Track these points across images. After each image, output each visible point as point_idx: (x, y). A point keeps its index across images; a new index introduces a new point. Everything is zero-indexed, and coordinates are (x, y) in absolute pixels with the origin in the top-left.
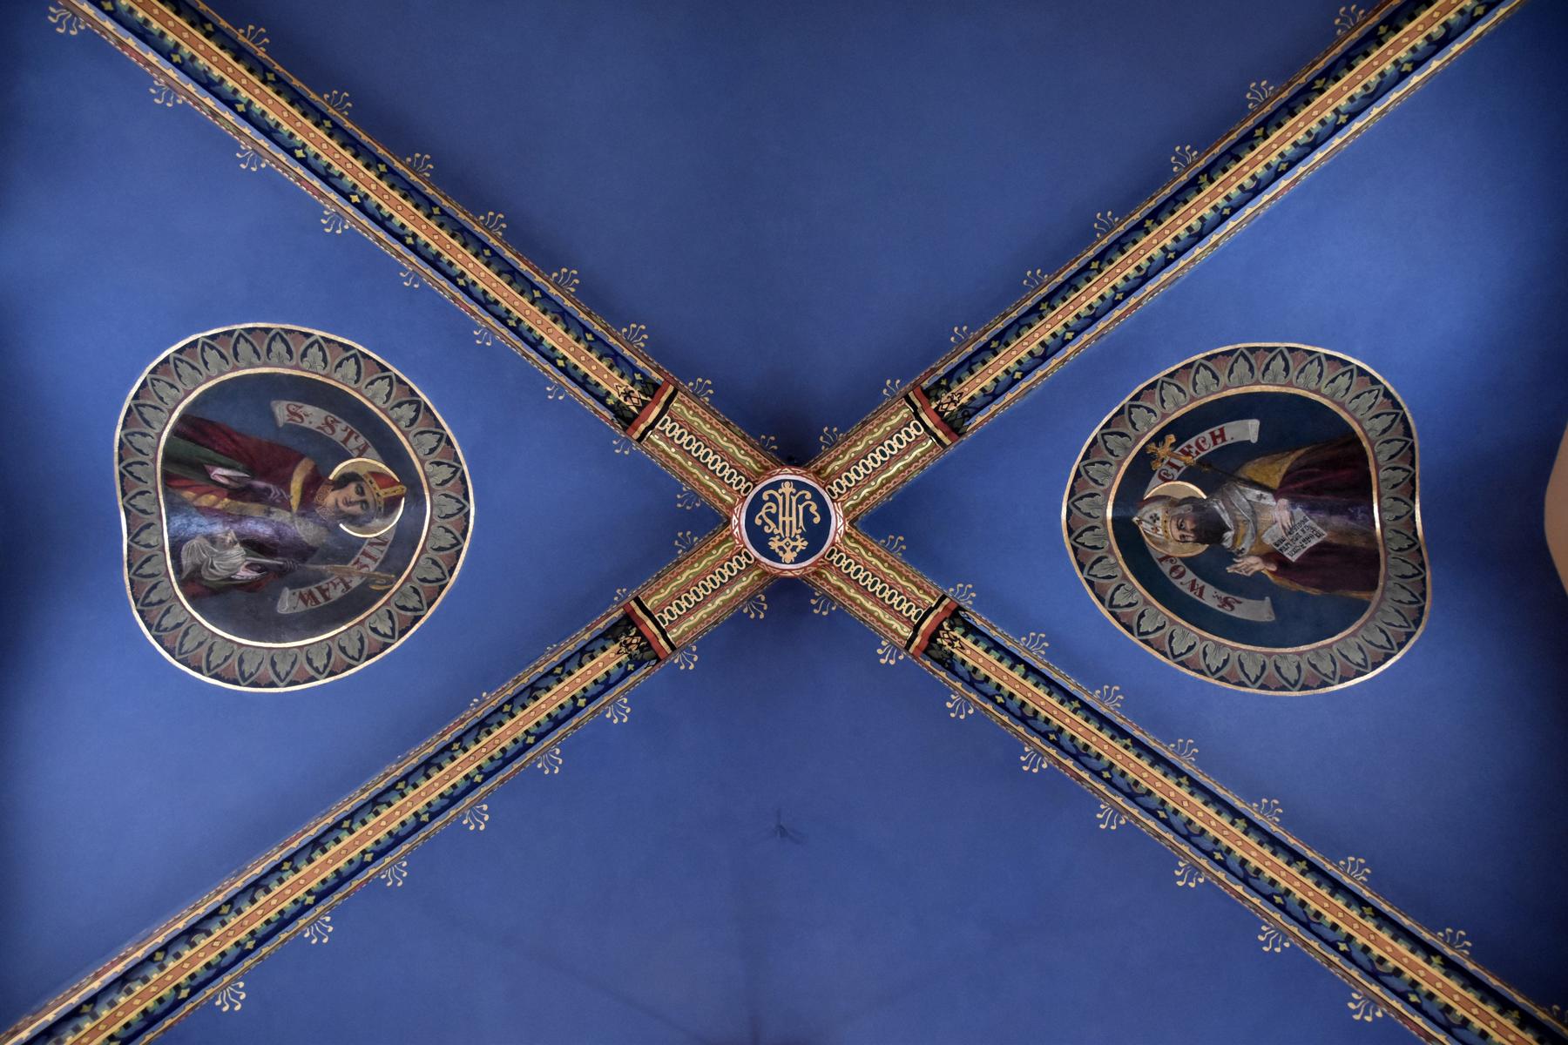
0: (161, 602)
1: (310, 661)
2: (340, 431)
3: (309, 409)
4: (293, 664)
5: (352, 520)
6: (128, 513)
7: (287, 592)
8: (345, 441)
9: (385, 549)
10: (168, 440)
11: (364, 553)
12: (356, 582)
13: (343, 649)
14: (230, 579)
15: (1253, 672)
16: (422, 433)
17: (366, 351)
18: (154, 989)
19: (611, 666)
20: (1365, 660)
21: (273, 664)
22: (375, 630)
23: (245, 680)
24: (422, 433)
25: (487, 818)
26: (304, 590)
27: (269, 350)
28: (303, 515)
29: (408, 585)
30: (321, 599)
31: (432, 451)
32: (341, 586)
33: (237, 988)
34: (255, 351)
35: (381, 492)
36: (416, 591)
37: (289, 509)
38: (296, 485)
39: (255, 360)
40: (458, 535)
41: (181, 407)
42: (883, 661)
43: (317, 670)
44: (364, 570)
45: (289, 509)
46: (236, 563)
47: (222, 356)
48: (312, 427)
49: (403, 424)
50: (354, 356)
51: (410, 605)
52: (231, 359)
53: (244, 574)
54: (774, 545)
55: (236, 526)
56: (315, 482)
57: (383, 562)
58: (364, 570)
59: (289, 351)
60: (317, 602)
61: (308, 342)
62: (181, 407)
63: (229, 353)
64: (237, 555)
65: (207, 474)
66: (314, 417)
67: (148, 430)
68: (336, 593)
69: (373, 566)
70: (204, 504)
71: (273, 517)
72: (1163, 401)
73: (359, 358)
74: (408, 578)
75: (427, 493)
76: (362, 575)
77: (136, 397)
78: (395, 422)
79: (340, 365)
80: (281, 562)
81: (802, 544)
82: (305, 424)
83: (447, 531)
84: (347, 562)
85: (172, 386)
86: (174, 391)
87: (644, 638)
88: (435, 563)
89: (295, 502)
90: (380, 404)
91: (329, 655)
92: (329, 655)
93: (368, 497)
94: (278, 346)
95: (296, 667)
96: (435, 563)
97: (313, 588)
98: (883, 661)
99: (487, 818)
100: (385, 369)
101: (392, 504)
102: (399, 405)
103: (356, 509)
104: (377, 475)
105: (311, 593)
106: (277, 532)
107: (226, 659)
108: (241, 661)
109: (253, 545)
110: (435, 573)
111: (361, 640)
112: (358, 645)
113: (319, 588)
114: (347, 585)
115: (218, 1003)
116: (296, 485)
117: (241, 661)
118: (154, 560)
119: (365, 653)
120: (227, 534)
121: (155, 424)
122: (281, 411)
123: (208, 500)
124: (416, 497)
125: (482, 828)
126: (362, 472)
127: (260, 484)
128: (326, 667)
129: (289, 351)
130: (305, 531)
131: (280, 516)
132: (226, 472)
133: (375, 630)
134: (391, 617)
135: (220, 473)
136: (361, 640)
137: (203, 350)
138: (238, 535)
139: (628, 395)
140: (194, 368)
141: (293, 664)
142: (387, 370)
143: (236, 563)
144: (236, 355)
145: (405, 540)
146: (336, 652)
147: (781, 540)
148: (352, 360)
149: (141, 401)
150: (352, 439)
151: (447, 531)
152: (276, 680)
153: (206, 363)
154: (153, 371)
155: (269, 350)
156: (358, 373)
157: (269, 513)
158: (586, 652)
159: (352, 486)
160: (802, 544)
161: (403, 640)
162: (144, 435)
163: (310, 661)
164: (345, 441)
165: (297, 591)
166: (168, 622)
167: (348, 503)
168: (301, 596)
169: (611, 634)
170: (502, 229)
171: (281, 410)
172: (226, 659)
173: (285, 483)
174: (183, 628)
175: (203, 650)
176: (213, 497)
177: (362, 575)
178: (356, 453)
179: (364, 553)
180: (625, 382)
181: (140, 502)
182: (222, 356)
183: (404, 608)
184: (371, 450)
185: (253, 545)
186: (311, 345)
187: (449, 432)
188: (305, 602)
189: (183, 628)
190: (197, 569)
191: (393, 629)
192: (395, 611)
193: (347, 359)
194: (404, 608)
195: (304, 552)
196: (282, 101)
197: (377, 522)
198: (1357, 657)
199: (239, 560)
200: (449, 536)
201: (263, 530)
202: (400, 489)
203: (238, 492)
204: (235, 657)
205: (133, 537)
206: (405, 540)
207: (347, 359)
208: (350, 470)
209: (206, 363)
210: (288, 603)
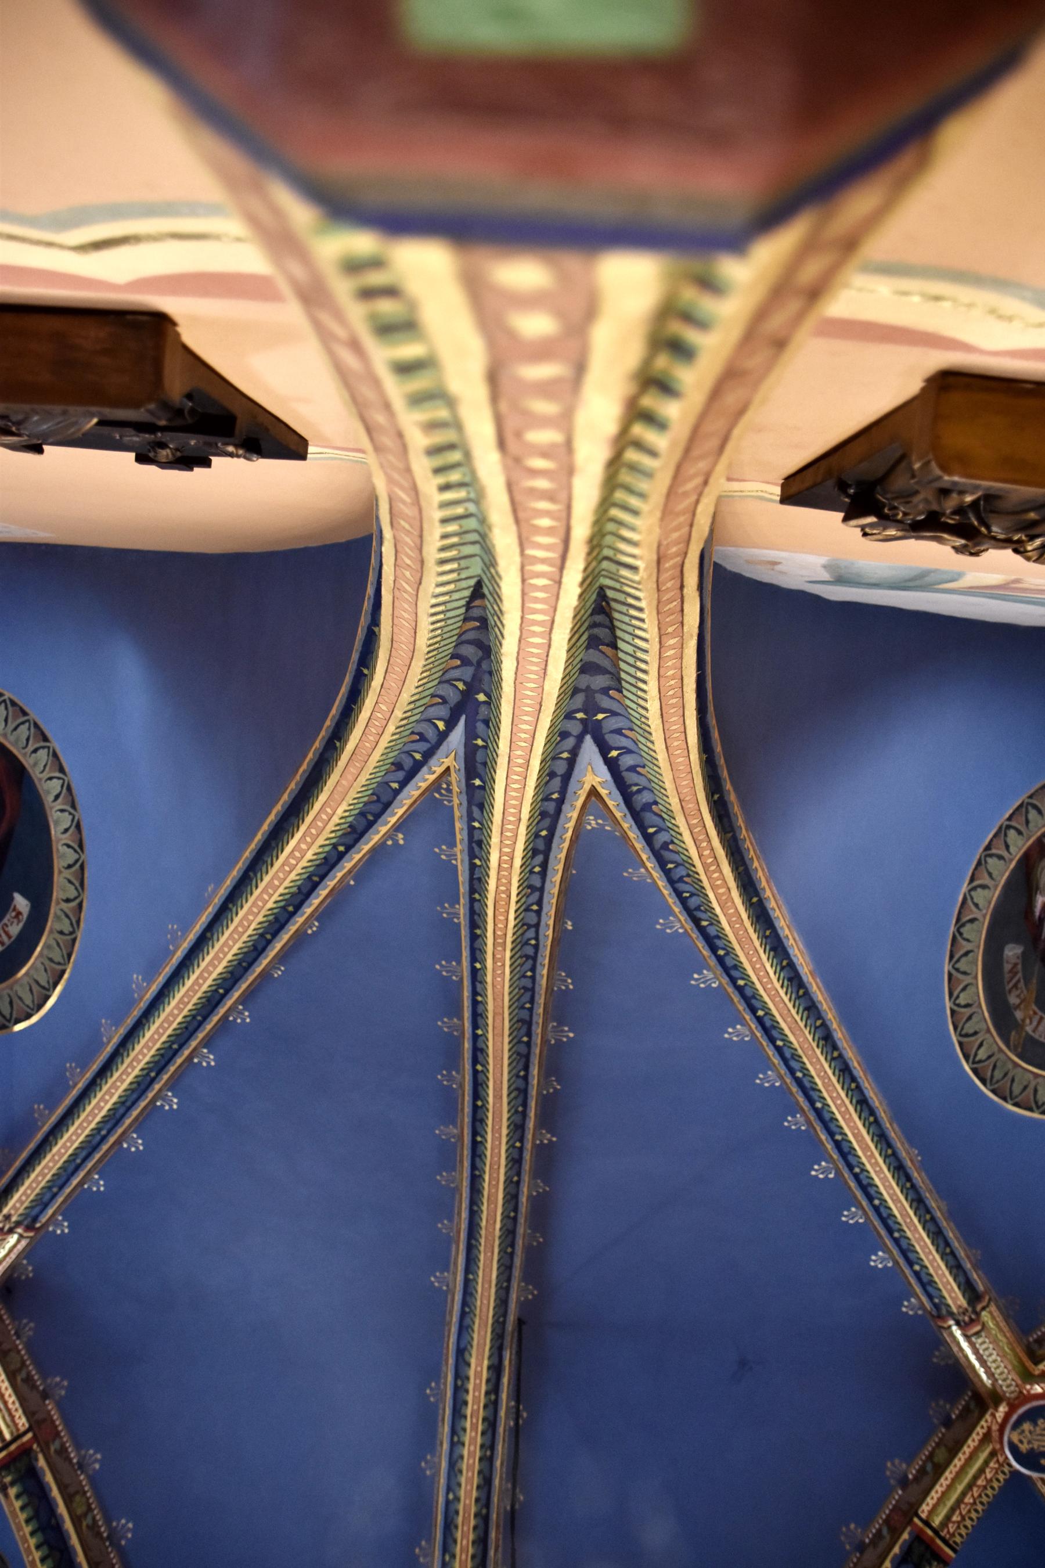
12: (1019, 1015)
15: (969, 1028)
20: (980, 1061)
42: (889, 1464)
44: (1028, 1021)
54: (1027, 1426)
57: (1031, 1038)
58: (1028, 1021)
74: (1016, 1065)
76: (1023, 1020)
81: (1024, 1448)
84: (1037, 1003)
91: (990, 874)
92: (990, 874)
97: (1020, 975)
98: (889, 1464)
114: (1018, 1007)
147: (1030, 1432)
160: (1024, 1448)
165: (1019, 961)
168: (1016, 965)
177: (1023, 1020)
198: (982, 1054)
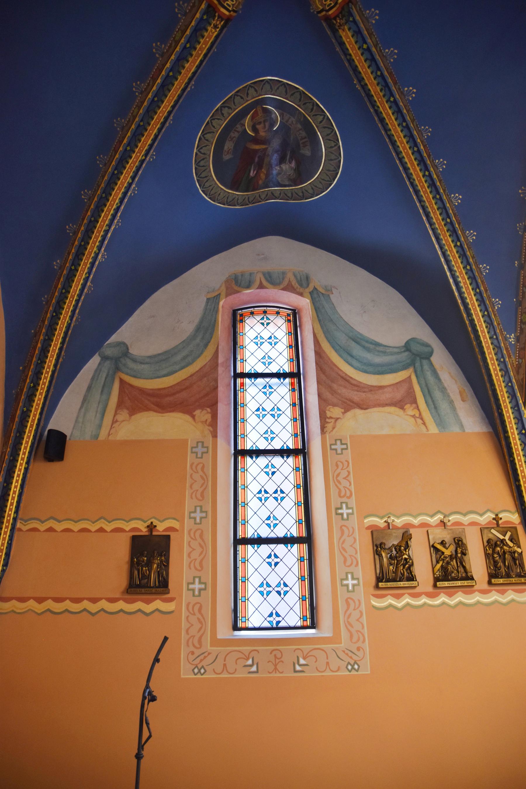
0: (303, 192)
1: (331, 147)
2: (234, 135)
3: (226, 148)
4: (332, 153)
5: (272, 125)
6: (266, 200)
7: (302, 151)
8: (238, 132)
9: (285, 114)
10: (240, 192)
11: (287, 122)
12: (299, 126)
13: (328, 135)
14: (295, 170)
16: (234, 103)
17: (201, 131)
18: (443, 233)
19: (350, 34)
21: (331, 160)
22: (321, 122)
23: (336, 170)
24: (234, 103)
25: (411, 88)
26: (301, 145)
27: (203, 166)
28: (269, 144)
29: (302, 106)
30: (306, 140)
31: (242, 98)
32: (301, 131)
33: (453, 197)
34: (204, 171)
35: (260, 115)
36: (305, 104)
37: (267, 149)
38: (257, 147)
39: (208, 170)
40: (279, 84)
41: (227, 190)
43: (335, 146)
44: (294, 123)
45: (267, 149)
46: (288, 167)
47: (207, 181)
48: (233, 145)
49: (230, 111)
50: (203, 136)
51: (311, 107)
52: (208, 178)
53: (293, 165)
55: (273, 166)
56: (256, 140)
58: (294, 123)
59: (203, 159)
60: (307, 141)
61: (199, 153)
62: (227, 190)
63: (205, 179)
64: (284, 167)
65: (252, 178)
66: (229, 145)
67: (236, 199)
68: (304, 134)
69: (292, 119)
70: (264, 177)
71: (270, 154)
72: (262, 89)
73: (203, 134)
75: (261, 97)
77: (224, 204)
78: (230, 114)
79: (207, 140)
80: (289, 150)
82: (232, 148)
83: (278, 88)
85: (220, 194)
86: (221, 194)
87: (338, 16)
88: (292, 95)
89: (264, 147)
90: (223, 122)
92: (330, 140)
93: (262, 120)
94: (202, 163)
95: (333, 152)
96: (292, 95)
99: (411, 88)
100: (208, 123)
101: (266, 111)
102: (223, 114)
103: (267, 124)
104: (253, 118)
105: (303, 143)
106: (277, 152)
107: (327, 175)
108: (329, 170)
109: (282, 160)
110: (297, 95)
111: (325, 127)
112: (326, 129)
113: (301, 140)
115: (457, 204)
116: (257, 147)
117: (329, 170)
118: (286, 193)
119: (330, 127)
120: (276, 169)
121: (234, 197)
122: (226, 157)
123: (263, 176)
124: (264, 101)
125: (415, 90)
126: (251, 124)
127: (256, 160)
128: (334, 142)
129: (203, 159)
130: (276, 143)
131: (270, 151)
132: (252, 172)
133: (321, 122)
134: (316, 115)
135: (252, 174)
136: (325, 127)
137: (205, 188)
138: (277, 165)
139: (216, 27)
140: (212, 189)
141: (332, 153)
142: (208, 121)
143: (288, 167)
144: (206, 177)
145: (280, 105)
146: (329, 137)
148: (205, 136)
149: (225, 203)
150: (237, 130)
151: (278, 88)
152: (338, 160)
153: (210, 186)
154: (214, 201)
155: (203, 166)
156: (210, 133)
157: (268, 155)
158: (342, 44)
159: (257, 126)
161: (326, 111)
162: (238, 199)
163: (331, 147)
164: (238, 132)
166: (311, 191)
167: (265, 127)
168: (304, 147)
169: (335, 31)
170: (141, 84)
171: (226, 157)
172: (327, 175)
173: (256, 151)
174: (314, 187)
175: (323, 182)
176: (262, 175)
178: (243, 127)
179: (287, 122)
180: (209, 28)
181: (263, 197)
182: (207, 181)
183: (312, 110)
184: (242, 122)
185: (282, 160)
186: (200, 152)
187: (233, 92)
188: (306, 145)
189: (314, 187)
190: (290, 180)
191: (321, 115)
192: (313, 113)
193: (205, 138)
194: (312, 110)
195: (285, 145)
196: (113, 193)
197: (273, 116)
199: (287, 166)
200: (280, 88)
201: (275, 158)
202: (259, 109)
203: (260, 166)
204: (327, 172)
205: (276, 198)
206: (280, 105)
207: (205, 138)
208: (250, 128)
209: (210, 186)
210: (307, 152)
